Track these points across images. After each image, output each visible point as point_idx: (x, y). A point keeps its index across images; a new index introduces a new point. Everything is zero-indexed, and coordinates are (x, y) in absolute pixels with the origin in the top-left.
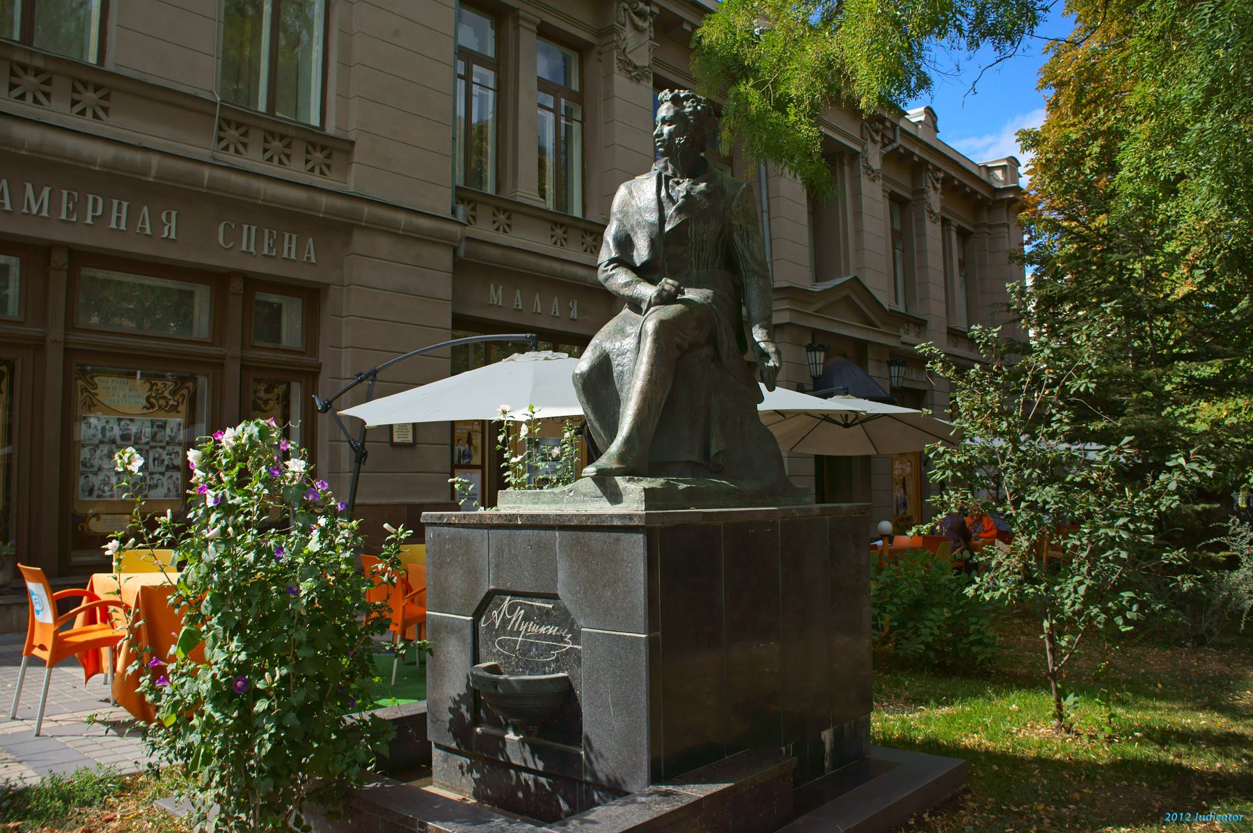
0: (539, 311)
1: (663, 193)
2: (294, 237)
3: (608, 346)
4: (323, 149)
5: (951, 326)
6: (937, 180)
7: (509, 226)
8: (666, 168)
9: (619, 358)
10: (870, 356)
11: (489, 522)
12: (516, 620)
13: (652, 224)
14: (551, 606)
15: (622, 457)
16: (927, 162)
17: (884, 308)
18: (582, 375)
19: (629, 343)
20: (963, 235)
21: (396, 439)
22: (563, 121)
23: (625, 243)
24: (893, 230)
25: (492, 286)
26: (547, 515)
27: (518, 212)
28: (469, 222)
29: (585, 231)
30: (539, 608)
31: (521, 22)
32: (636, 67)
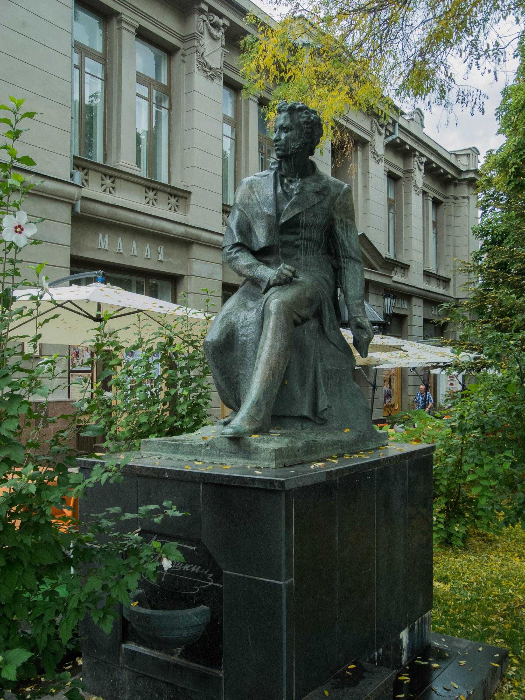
0: (135, 254)
1: (279, 190)
5: (426, 269)
6: (422, 163)
7: (113, 188)
9: (243, 330)
11: (138, 472)
13: (269, 216)
14: (194, 548)
15: (252, 418)
16: (415, 150)
17: (380, 255)
18: (212, 343)
19: (252, 316)
20: (437, 203)
22: (154, 108)
24: (389, 199)
27: (120, 178)
28: (83, 184)
31: (124, 25)
32: (211, 69)
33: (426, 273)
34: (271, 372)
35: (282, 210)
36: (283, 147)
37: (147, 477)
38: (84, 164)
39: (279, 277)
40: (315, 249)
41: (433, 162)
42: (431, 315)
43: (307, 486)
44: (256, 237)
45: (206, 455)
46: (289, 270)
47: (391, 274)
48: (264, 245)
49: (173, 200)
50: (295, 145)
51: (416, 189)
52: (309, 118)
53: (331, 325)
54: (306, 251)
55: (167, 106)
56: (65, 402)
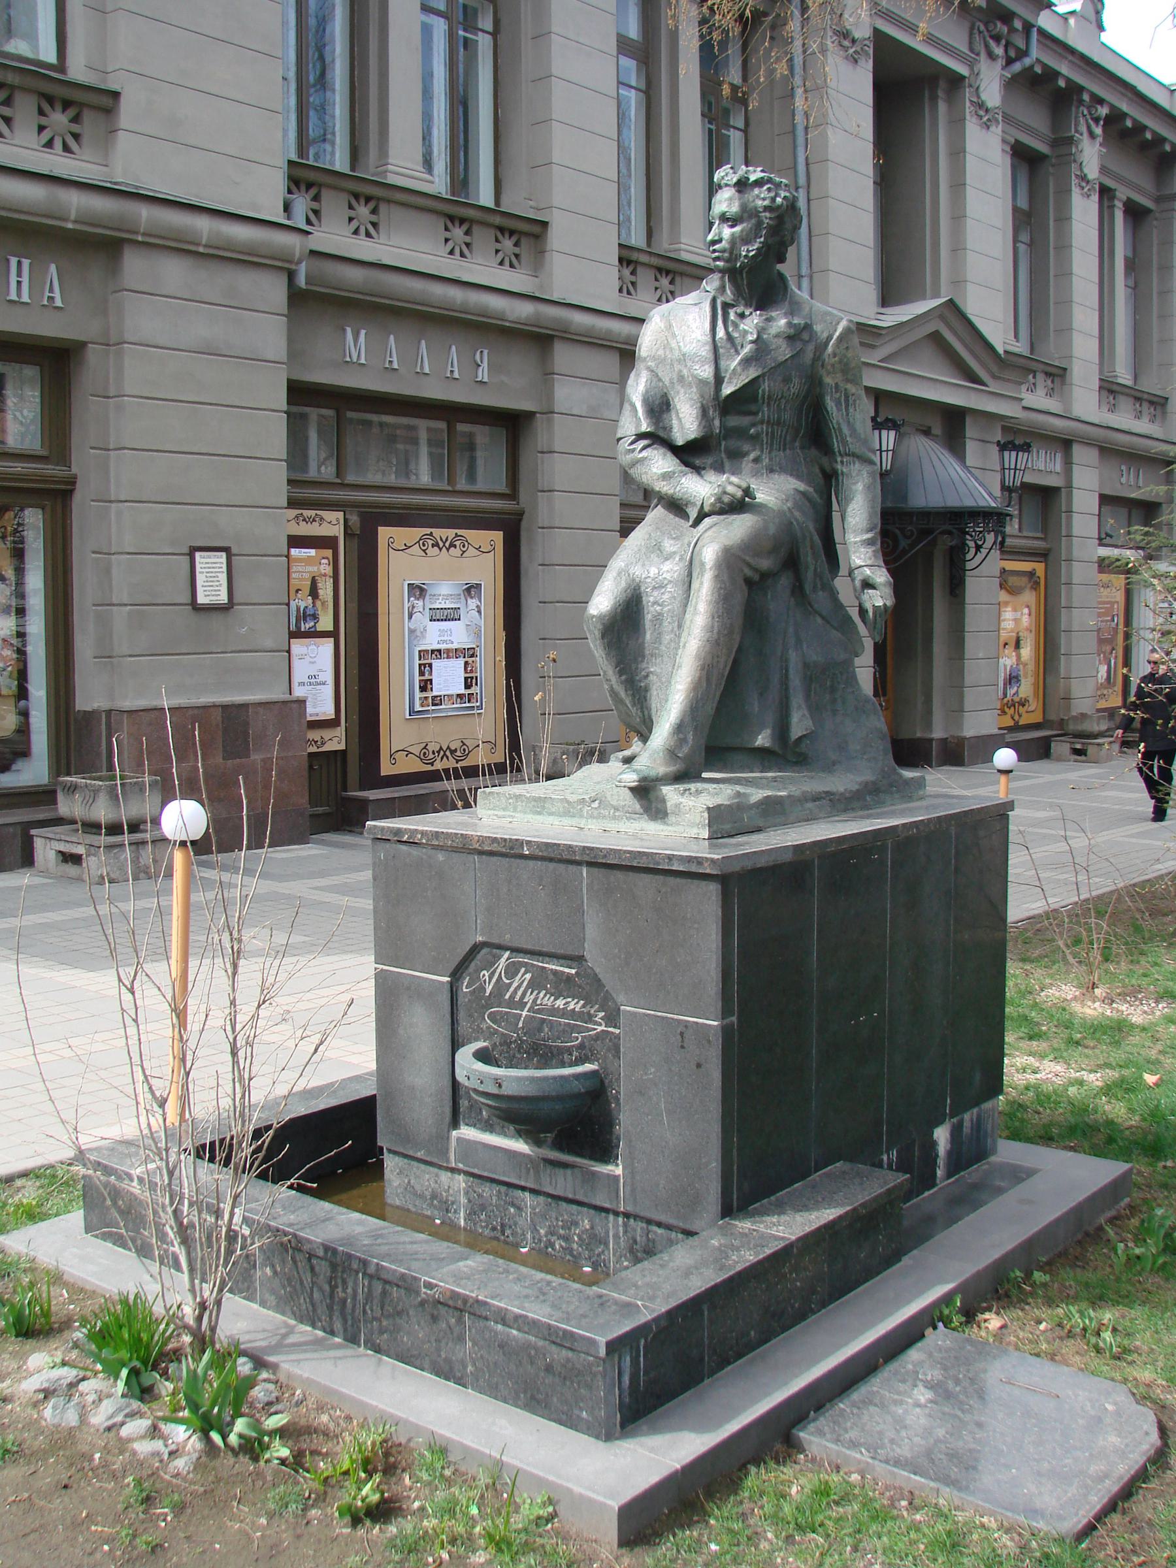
1: (721, 333)
2: (26, 263)
3: (637, 571)
4: (67, 104)
6: (1096, 120)
8: (722, 289)
9: (655, 593)
10: (969, 432)
11: (477, 846)
12: (519, 987)
13: (702, 382)
15: (671, 754)
16: (1081, 89)
19: (671, 570)
20: (1135, 214)
21: (202, 599)
23: (659, 407)
24: (1016, 210)
25: (349, 330)
26: (570, 846)
27: (389, 201)
29: (501, 229)
30: (555, 973)
33: (1106, 385)
34: (704, 673)
35: (726, 371)
36: (726, 255)
37: (491, 853)
38: (312, 176)
39: (719, 500)
40: (788, 438)
41: (1124, 115)
42: (1118, 486)
43: (761, 869)
44: (679, 419)
45: (592, 817)
46: (739, 487)
47: (1020, 393)
48: (693, 437)
49: (508, 244)
50: (749, 250)
51: (1084, 184)
52: (773, 200)
53: (818, 580)
54: (772, 445)
55: (489, 26)
56: (284, 702)
